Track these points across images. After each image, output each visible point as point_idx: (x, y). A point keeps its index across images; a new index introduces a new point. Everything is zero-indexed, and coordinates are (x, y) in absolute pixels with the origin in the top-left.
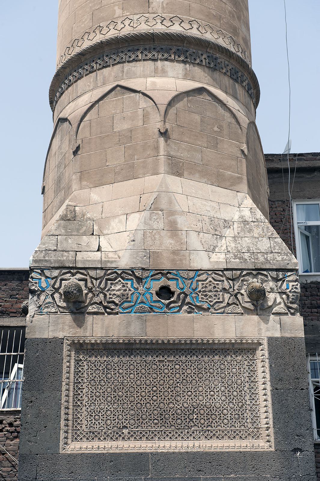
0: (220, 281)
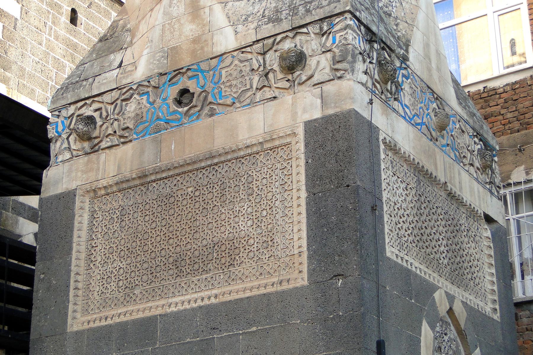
0: (247, 60)
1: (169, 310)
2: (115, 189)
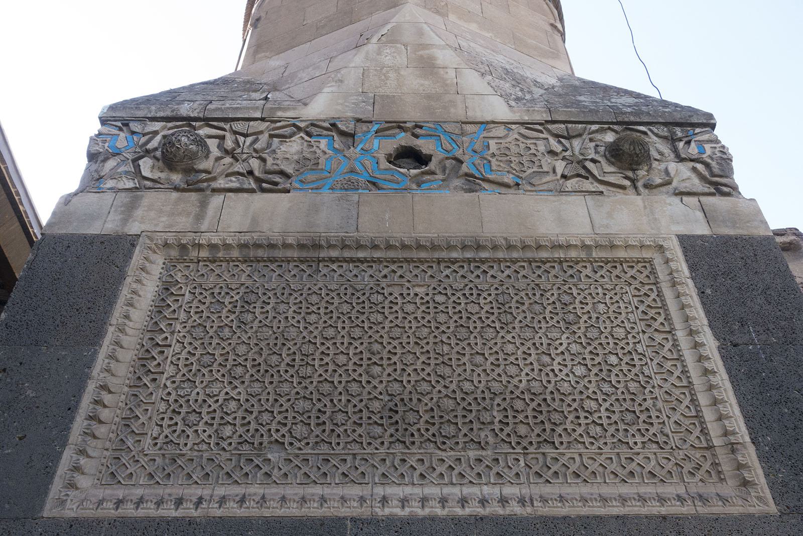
1: (382, 512)
2: (235, 254)
